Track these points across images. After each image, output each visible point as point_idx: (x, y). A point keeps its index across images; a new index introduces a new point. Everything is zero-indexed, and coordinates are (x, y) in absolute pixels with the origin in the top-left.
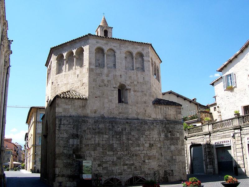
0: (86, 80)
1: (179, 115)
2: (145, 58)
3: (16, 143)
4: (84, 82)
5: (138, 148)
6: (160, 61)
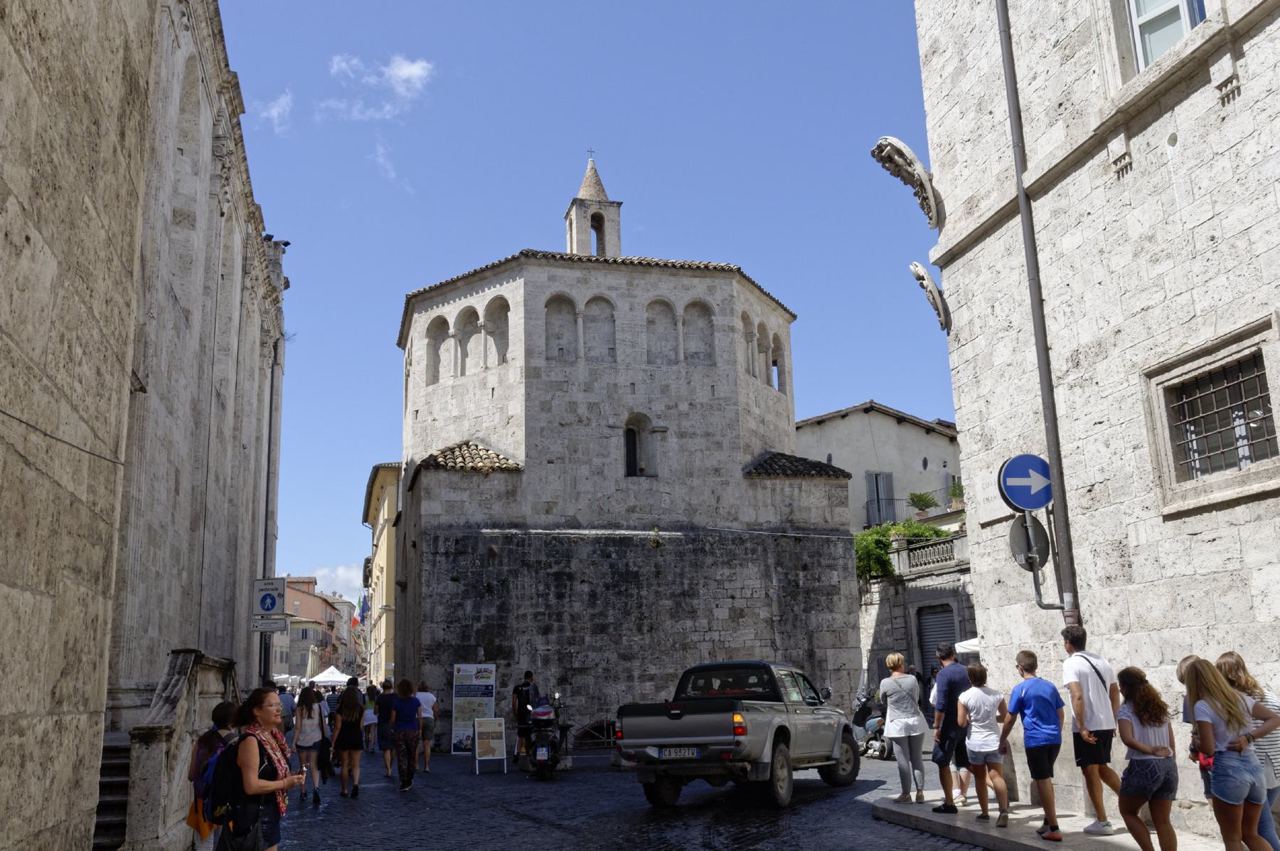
0: (517, 407)
1: (838, 510)
2: (718, 320)
3: (334, 593)
4: (510, 413)
5: (689, 623)
6: (787, 316)
